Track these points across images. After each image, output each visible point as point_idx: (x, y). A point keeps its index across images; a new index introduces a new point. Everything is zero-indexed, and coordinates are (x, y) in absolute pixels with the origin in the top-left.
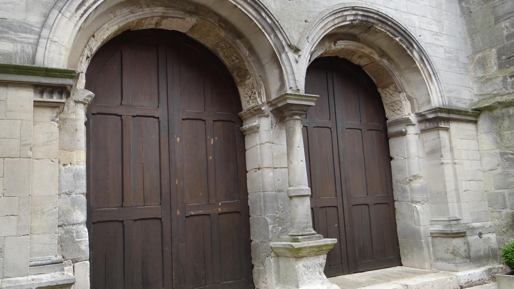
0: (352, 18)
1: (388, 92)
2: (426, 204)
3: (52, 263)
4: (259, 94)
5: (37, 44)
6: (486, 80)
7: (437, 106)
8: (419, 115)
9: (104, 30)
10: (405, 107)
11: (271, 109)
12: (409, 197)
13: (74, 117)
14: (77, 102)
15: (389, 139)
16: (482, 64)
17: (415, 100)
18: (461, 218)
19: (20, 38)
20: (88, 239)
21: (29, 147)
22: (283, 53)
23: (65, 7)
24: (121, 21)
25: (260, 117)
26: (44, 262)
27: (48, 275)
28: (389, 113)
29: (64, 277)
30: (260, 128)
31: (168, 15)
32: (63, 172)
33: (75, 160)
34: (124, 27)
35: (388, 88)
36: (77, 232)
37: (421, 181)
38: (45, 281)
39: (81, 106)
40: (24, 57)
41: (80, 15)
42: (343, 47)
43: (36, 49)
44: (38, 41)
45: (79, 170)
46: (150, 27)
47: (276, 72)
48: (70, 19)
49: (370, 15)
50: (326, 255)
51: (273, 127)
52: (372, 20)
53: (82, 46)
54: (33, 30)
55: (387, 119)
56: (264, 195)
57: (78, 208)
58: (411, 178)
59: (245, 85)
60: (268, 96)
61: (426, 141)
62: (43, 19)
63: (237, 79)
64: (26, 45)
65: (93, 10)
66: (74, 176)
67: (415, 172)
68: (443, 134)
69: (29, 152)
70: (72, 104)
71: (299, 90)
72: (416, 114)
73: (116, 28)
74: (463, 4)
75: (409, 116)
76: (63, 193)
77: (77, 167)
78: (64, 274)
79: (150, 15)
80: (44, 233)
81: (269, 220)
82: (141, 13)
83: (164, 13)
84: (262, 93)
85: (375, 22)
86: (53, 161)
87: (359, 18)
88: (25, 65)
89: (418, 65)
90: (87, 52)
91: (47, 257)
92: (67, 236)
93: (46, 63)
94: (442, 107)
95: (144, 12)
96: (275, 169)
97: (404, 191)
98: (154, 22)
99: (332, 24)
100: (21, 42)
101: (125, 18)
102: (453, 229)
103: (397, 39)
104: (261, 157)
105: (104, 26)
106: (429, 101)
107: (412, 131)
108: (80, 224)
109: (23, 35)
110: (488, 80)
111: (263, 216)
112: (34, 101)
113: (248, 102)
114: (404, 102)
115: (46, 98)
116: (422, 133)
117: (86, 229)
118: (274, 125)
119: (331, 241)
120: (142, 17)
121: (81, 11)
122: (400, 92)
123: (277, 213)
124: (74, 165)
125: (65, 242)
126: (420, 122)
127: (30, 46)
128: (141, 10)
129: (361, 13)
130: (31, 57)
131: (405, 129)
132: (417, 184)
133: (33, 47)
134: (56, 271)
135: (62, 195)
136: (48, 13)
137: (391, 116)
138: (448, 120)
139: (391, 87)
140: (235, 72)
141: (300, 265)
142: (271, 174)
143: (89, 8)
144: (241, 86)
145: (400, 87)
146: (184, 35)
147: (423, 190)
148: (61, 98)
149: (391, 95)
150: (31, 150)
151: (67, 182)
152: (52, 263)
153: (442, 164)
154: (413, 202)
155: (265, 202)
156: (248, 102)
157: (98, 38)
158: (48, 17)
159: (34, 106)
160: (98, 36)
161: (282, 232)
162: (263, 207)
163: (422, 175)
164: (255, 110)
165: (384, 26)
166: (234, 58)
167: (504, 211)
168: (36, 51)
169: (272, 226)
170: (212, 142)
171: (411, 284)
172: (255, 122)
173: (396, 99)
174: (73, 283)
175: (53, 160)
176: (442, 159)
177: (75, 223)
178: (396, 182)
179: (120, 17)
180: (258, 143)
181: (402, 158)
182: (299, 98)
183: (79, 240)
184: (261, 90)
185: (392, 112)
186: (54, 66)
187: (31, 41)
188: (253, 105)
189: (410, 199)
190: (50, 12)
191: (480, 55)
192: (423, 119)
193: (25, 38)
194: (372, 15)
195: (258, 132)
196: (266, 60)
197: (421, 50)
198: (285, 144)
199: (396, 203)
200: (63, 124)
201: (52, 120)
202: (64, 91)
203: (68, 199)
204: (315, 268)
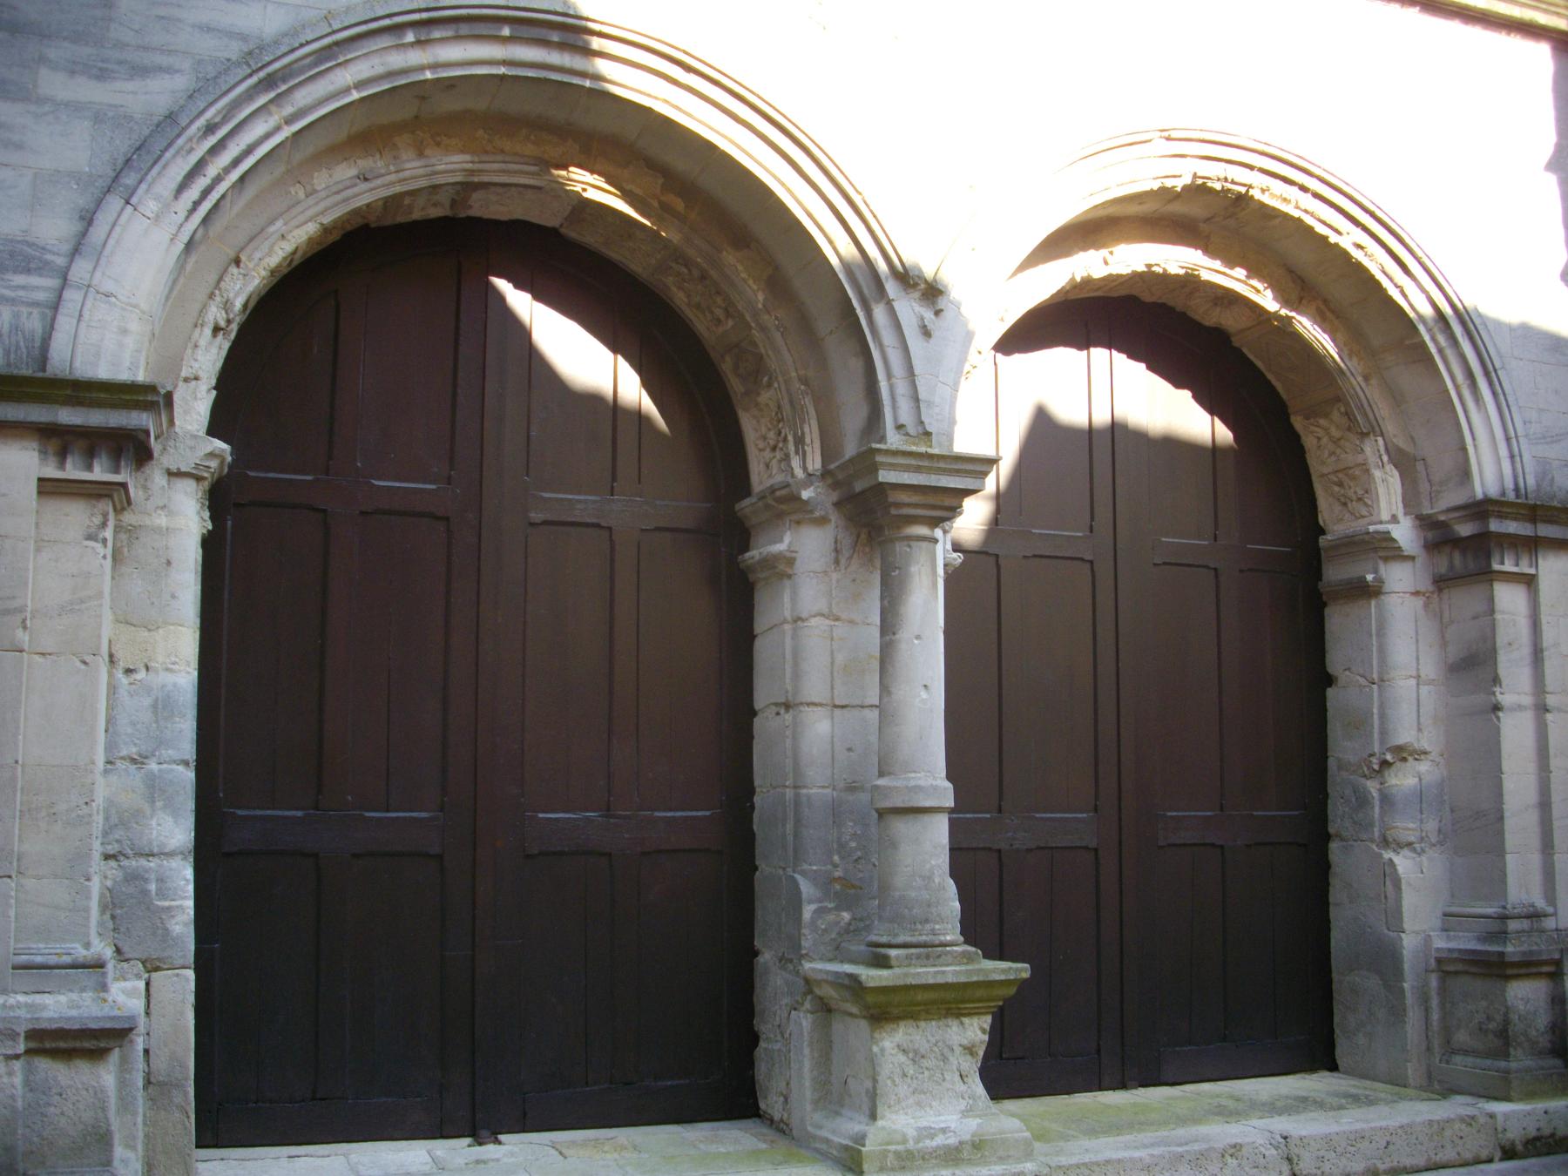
1: (1326, 430)
2: (1431, 853)
3: (74, 966)
4: (799, 441)
5: (55, 307)
7: (1493, 491)
8: (1426, 523)
9: (271, 240)
10: (1381, 490)
11: (835, 497)
12: (1372, 825)
13: (162, 520)
14: (174, 474)
15: (1325, 605)
17: (1420, 466)
18: (1550, 910)
19: (9, 287)
20: (191, 903)
21: (19, 618)
22: (877, 302)
23: (143, 186)
24: (326, 209)
25: (798, 523)
26: (53, 960)
27: (63, 998)
28: (1327, 511)
29: (106, 1011)
30: (798, 563)
31: (486, 179)
32: (123, 693)
33: (160, 659)
34: (335, 225)
35: (1326, 415)
36: (160, 880)
37: (1424, 767)
38: (51, 1014)
39: (190, 485)
40: (18, 347)
41: (189, 205)
43: (53, 319)
44: (60, 297)
45: (170, 688)
46: (434, 213)
47: (857, 365)
48: (157, 218)
50: (989, 1019)
51: (843, 561)
53: (202, 296)
54: (47, 263)
55: (1322, 532)
56: (797, 796)
57: (165, 807)
58: (1389, 757)
59: (757, 405)
61: (1452, 622)
62: (77, 227)
63: (736, 385)
64: (24, 310)
65: (233, 186)
66: (155, 706)
67: (1405, 735)
69: (20, 633)
70: (159, 479)
71: (928, 434)
73: (311, 229)
75: (1390, 527)
76: (122, 758)
77: (169, 679)
78: (105, 1000)
79: (423, 183)
80: (56, 876)
81: (806, 888)
82: (393, 177)
83: (472, 172)
84: (808, 440)
86: (85, 663)
88: (15, 372)
89: (1427, 338)
90: (215, 314)
91: (59, 947)
92: (131, 890)
93: (77, 364)
94: (1511, 496)
95: (401, 175)
96: (837, 712)
97: (1363, 801)
98: (444, 198)
100: (12, 301)
101: (338, 198)
102: (1510, 949)
104: (796, 664)
105: (272, 229)
106: (1465, 474)
108: (171, 855)
109: (20, 279)
111: (789, 871)
112: (40, 480)
113: (767, 466)
114: (1377, 474)
115: (73, 471)
116: (1440, 590)
117: (189, 872)
118: (846, 553)
120: (398, 189)
121: (193, 193)
122: (1364, 435)
123: (836, 866)
124: (157, 672)
125: (127, 908)
126: (1432, 547)
127: (36, 311)
128: (392, 168)
130: (38, 344)
131: (1376, 571)
132: (1403, 780)
133: (43, 315)
134: (83, 990)
135: (121, 765)
136: (92, 206)
137: (1335, 522)
138: (1533, 545)
139: (1335, 415)
140: (728, 358)
141: (892, 1045)
143: (218, 180)
144: (746, 410)
145: (1365, 415)
146: (553, 233)
148: (117, 471)
149: (1336, 442)
150: (25, 628)
151: (133, 724)
152: (74, 966)
154: (1385, 843)
155: (798, 821)
156: (767, 466)
157: (251, 265)
158: (90, 222)
159: (40, 493)
160: (250, 259)
161: (849, 931)
162: (790, 838)
163: (1428, 749)
164: (781, 500)
166: (719, 312)
168: (52, 327)
169: (813, 907)
171: (1304, 1133)
172: (781, 541)
173: (1350, 459)
174: (131, 1029)
175: (88, 658)
176: (1497, 690)
177: (156, 850)
178: (1340, 768)
179: (323, 194)
180: (787, 614)
181: (1362, 680)
182: (926, 463)
183: (166, 904)
184: (807, 429)
185: (1337, 508)
186: (103, 373)
187: (41, 296)
188: (779, 478)
189: (1377, 834)
190: (99, 203)
192: (1438, 537)
193: (23, 288)
195: (789, 577)
196: (826, 325)
198: (877, 619)
199: (1334, 846)
200: (130, 544)
201: (90, 537)
202: (133, 449)
203: (135, 777)
204: (945, 1059)
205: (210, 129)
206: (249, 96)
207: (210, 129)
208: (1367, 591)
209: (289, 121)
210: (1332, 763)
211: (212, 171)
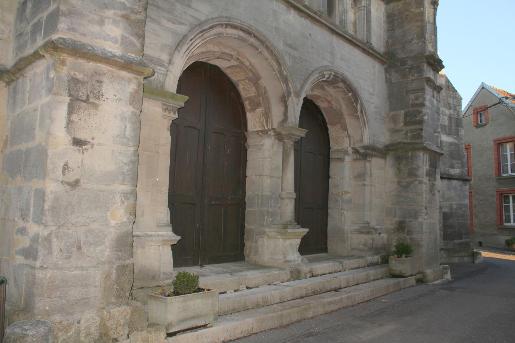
6: (394, 131)
8: (354, 149)
11: (274, 134)
14: (365, 153)
16: (394, 119)
35: (336, 126)
37: (349, 195)
60: (272, 126)
68: (368, 165)
72: (352, 148)
74: (387, 75)
106: (362, 141)
107: (348, 159)
110: (396, 131)
119: (306, 230)
121: (187, 53)
132: (347, 197)
133: (163, 77)
138: (372, 156)
142: (269, 181)
147: (349, 201)
153: (364, 185)
167: (394, 220)
170: (228, 152)
187: (163, 72)
191: (392, 113)
192: (356, 151)
197: (362, 105)
205: (191, 40)
206: (198, 34)
207: (191, 40)
208: (341, 160)
209: (203, 40)
210: (330, 193)
211: (190, 49)
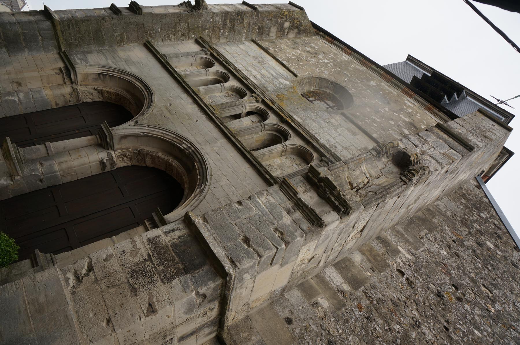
0: (186, 147)
42: (176, 166)
49: (197, 154)
52: (195, 157)
65: (75, 304)
85: (197, 159)
87: (190, 151)
99: (170, 138)
103: (199, 177)
129: (193, 149)
165: (199, 165)
194: (199, 155)
197: (202, 191)
